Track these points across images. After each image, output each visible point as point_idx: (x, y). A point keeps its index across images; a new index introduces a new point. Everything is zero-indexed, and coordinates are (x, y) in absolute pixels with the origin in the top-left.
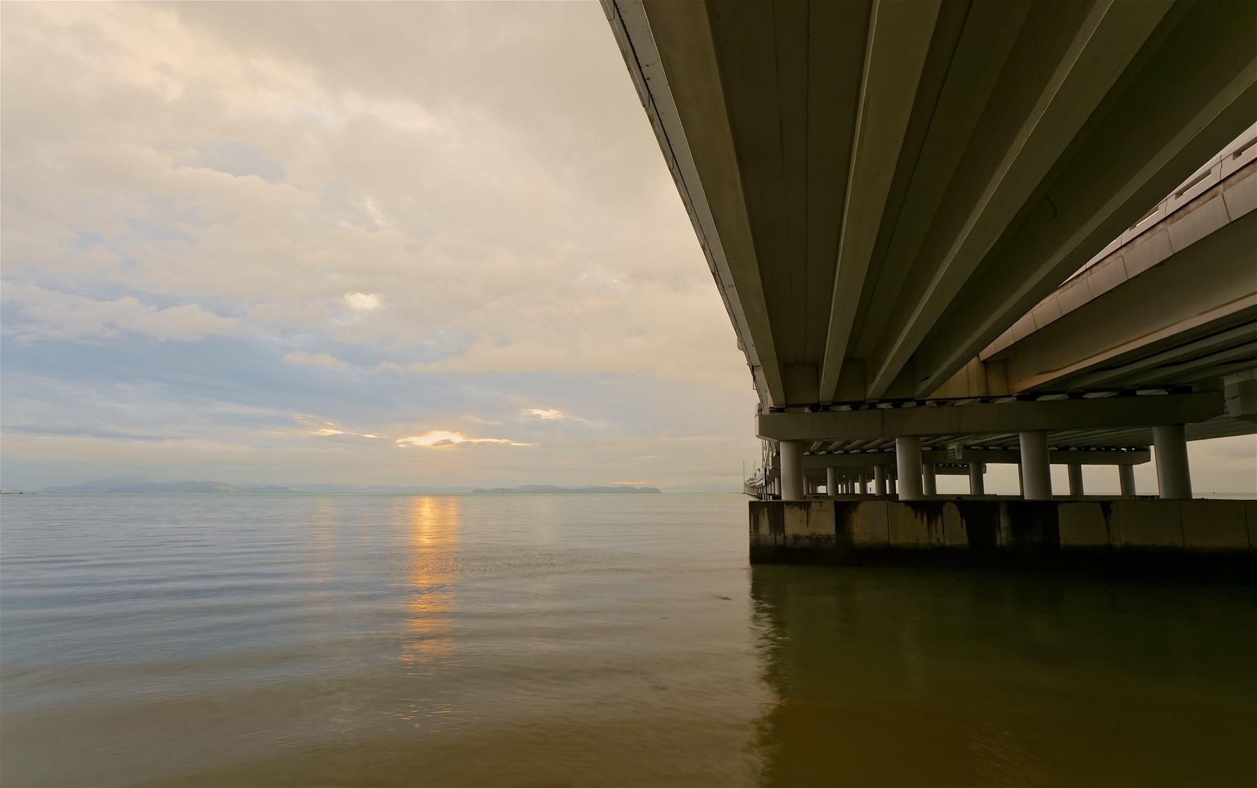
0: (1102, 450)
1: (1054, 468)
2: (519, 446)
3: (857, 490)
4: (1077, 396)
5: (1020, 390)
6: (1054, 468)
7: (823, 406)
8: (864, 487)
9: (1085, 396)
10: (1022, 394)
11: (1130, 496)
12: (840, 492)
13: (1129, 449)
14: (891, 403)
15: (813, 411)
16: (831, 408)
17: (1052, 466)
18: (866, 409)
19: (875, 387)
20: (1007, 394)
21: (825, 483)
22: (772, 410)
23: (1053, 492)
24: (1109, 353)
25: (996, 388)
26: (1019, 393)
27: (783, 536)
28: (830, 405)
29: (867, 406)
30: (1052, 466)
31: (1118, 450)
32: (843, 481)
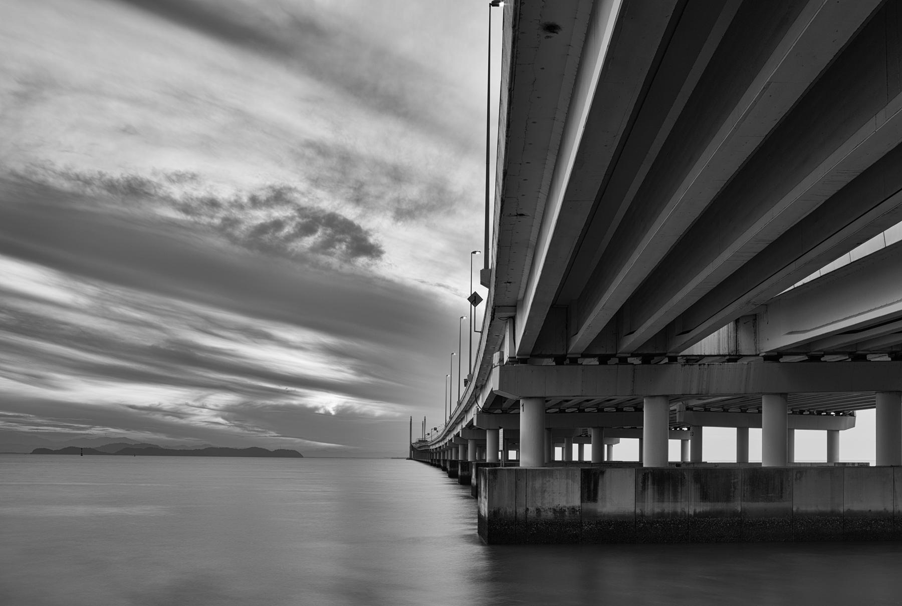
0: (814, 414)
1: (671, 442)
2: (329, 448)
3: (588, 456)
4: (815, 359)
5: (767, 350)
6: (671, 442)
7: (570, 358)
8: (568, 452)
9: (822, 359)
10: (769, 354)
11: (835, 463)
12: (606, 459)
13: (837, 413)
14: (640, 358)
15: (557, 364)
16: (580, 361)
17: (670, 441)
18: (616, 364)
19: (630, 342)
20: (754, 354)
21: (635, 431)
22: (512, 360)
23: (749, 459)
24: (821, 329)
25: (746, 348)
26: (766, 352)
27: (97, 180)
28: (579, 358)
29: (616, 360)
30: (670, 441)
31: (828, 414)
32: (674, 429)
